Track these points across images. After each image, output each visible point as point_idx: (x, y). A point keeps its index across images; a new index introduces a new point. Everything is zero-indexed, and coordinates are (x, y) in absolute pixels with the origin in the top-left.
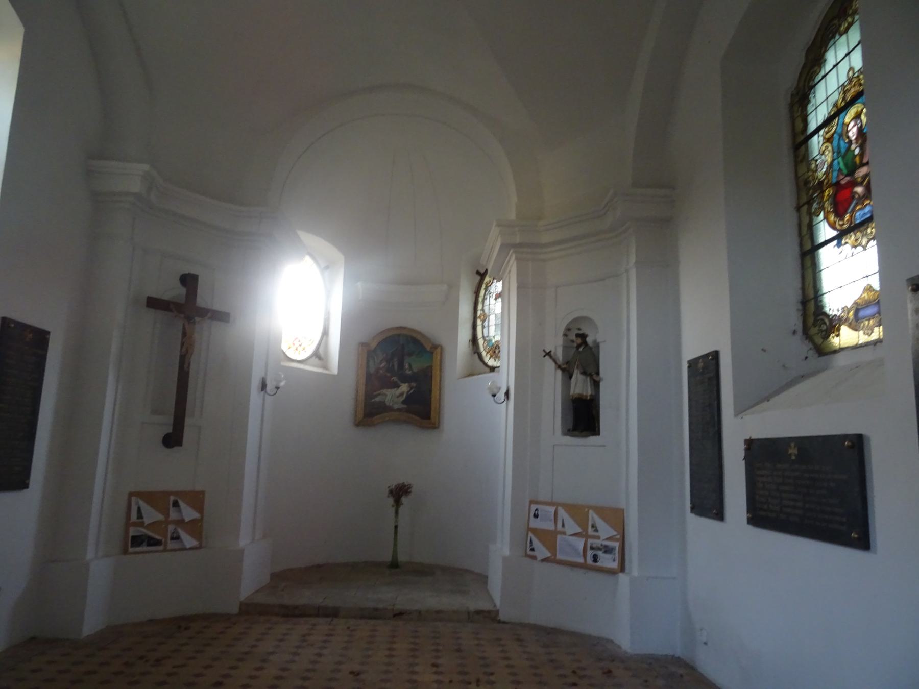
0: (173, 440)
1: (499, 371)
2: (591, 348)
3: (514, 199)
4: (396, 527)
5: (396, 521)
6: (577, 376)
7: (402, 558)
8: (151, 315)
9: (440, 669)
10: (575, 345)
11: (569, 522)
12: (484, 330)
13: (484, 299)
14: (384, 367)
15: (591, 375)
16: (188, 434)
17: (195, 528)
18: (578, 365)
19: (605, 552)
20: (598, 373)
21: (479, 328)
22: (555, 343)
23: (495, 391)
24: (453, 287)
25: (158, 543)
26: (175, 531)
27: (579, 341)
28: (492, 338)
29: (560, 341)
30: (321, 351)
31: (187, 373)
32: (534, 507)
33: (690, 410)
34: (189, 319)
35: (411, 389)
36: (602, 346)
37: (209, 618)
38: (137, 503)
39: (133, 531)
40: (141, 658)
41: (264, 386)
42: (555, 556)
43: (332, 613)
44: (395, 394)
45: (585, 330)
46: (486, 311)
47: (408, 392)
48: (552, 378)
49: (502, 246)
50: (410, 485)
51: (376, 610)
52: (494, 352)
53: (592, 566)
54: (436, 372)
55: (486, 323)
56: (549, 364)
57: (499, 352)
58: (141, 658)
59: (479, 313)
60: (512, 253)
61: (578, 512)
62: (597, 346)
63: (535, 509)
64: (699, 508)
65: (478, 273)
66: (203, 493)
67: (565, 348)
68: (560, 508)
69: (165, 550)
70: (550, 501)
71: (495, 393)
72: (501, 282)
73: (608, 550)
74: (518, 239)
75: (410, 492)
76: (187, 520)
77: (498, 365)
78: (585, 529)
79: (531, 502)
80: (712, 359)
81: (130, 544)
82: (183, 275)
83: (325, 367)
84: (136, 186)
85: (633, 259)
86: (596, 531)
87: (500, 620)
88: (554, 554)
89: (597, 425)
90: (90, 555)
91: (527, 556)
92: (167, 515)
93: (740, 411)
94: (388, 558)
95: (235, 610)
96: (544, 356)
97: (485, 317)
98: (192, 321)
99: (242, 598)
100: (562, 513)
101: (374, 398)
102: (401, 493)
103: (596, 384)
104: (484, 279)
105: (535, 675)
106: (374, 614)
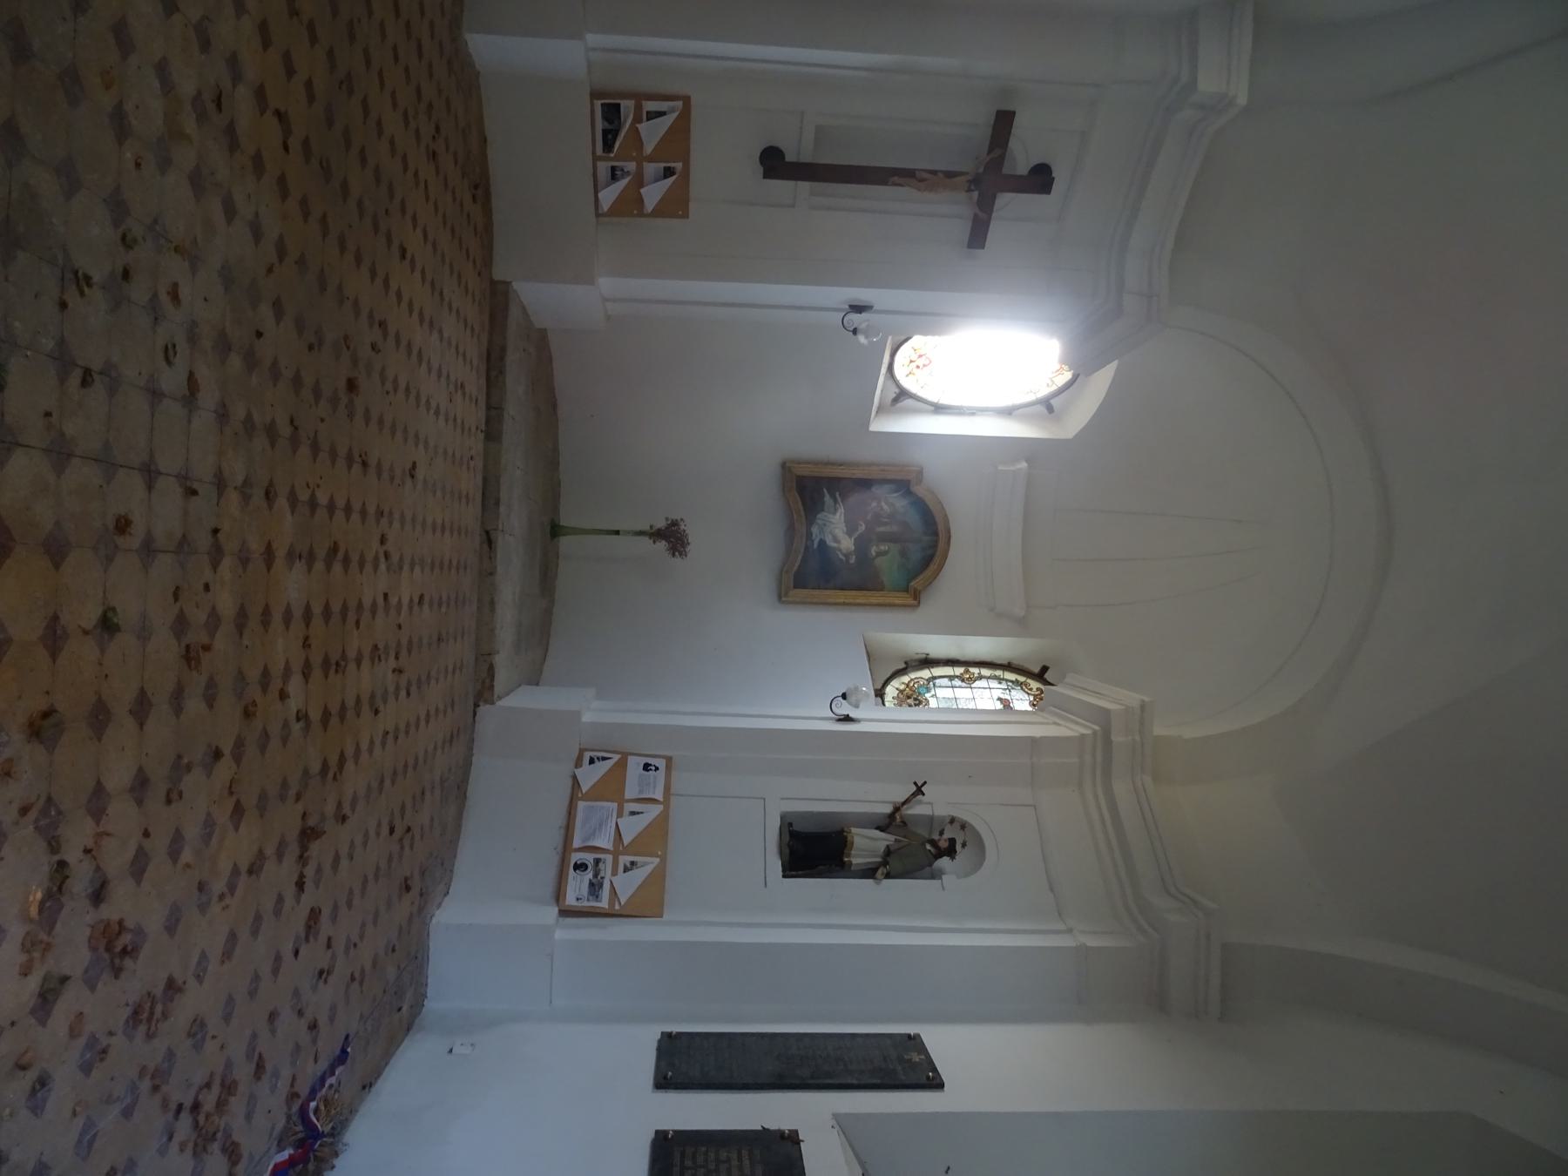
0: (774, 163)
1: (876, 705)
2: (930, 865)
3: (1189, 733)
4: (617, 533)
5: (628, 533)
6: (882, 840)
7: (565, 542)
8: (980, 118)
9: (416, 608)
10: (936, 837)
11: (640, 823)
12: (946, 680)
13: (1000, 680)
14: (882, 509)
15: (885, 863)
16: (782, 188)
17: (630, 205)
18: (900, 841)
19: (591, 884)
20: (888, 876)
21: (948, 671)
22: (938, 803)
23: (852, 698)
24: (1020, 625)
25: (608, 146)
26: (625, 173)
27: (944, 844)
28: (933, 692)
29: (942, 811)
30: (909, 402)
31: (884, 182)
32: (661, 763)
33: (867, 1035)
34: (975, 182)
35: (845, 555)
36: (935, 883)
37: (486, 234)
38: (673, 110)
39: (627, 106)
40: (438, 129)
41: (858, 309)
42: (582, 799)
43: (492, 432)
44: (836, 528)
45: (962, 855)
46: (977, 684)
47: (840, 550)
48: (878, 797)
49: (1107, 712)
50: (686, 556)
51: (497, 503)
52: (909, 697)
53: (566, 864)
54: (875, 597)
55: (957, 682)
56: (902, 792)
57: (910, 706)
58: (438, 129)
59: (975, 671)
60: (1093, 729)
61: (656, 838)
62: (936, 875)
63: (657, 765)
64: (671, 1047)
65: (1045, 669)
66: (686, 215)
67: (931, 820)
68: (661, 807)
69: (595, 159)
70: (672, 791)
71: (848, 697)
72: (1030, 709)
73: (595, 888)
74: (1117, 738)
75: (674, 555)
76: (642, 191)
77: (887, 704)
78: (626, 851)
79: (669, 760)
80: (928, 1077)
81: (603, 101)
82: (1050, 168)
83: (880, 410)
84: (1208, 84)
85: (1092, 942)
86: (626, 870)
87: (479, 706)
88: (586, 797)
89: (800, 872)
90: (593, 39)
91: (582, 751)
92: (651, 159)
93: (844, 1124)
94: (565, 521)
95: (499, 274)
96: (915, 783)
97: (969, 681)
98: (972, 187)
99: (515, 285)
100: (654, 811)
101: (829, 493)
102: (672, 540)
103: (869, 873)
104: (1033, 679)
105: (406, 766)
106: (490, 498)
